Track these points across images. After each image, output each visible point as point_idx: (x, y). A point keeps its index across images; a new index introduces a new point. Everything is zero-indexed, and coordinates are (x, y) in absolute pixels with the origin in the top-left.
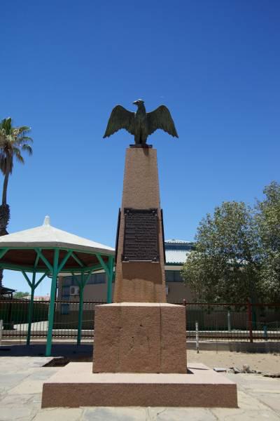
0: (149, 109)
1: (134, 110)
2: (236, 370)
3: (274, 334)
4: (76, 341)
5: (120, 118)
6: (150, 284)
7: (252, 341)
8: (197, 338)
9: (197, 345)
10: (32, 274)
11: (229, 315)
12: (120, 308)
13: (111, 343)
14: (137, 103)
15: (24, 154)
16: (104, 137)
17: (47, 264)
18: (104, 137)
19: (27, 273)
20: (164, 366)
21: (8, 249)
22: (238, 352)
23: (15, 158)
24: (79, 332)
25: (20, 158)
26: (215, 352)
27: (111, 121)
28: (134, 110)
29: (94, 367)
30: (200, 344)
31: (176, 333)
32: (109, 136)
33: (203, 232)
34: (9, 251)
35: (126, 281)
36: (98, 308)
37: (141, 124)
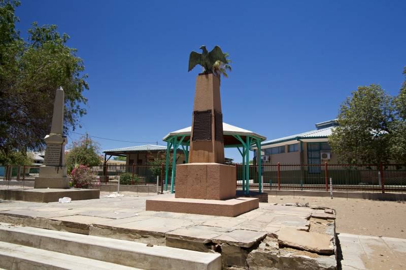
0: (209, 50)
1: (200, 52)
2: (299, 205)
3: (393, 187)
4: (242, 189)
5: (195, 59)
6: (206, 152)
7: (383, 193)
8: (331, 189)
9: (331, 193)
10: (242, 148)
11: (379, 173)
12: (187, 165)
13: (183, 184)
14: (201, 48)
15: (227, 71)
16: (189, 71)
17: (243, 142)
18: (189, 71)
19: (182, 149)
20: (208, 196)
21: (185, 136)
22: (370, 199)
23: (222, 75)
24: (383, 187)
25: (225, 75)
26: (346, 199)
27: (190, 61)
28: (200, 52)
29: (176, 195)
30: (333, 193)
31: (215, 179)
32: (191, 70)
33: (344, 111)
34: (186, 137)
35: (194, 151)
36: (179, 166)
37: (208, 61)
